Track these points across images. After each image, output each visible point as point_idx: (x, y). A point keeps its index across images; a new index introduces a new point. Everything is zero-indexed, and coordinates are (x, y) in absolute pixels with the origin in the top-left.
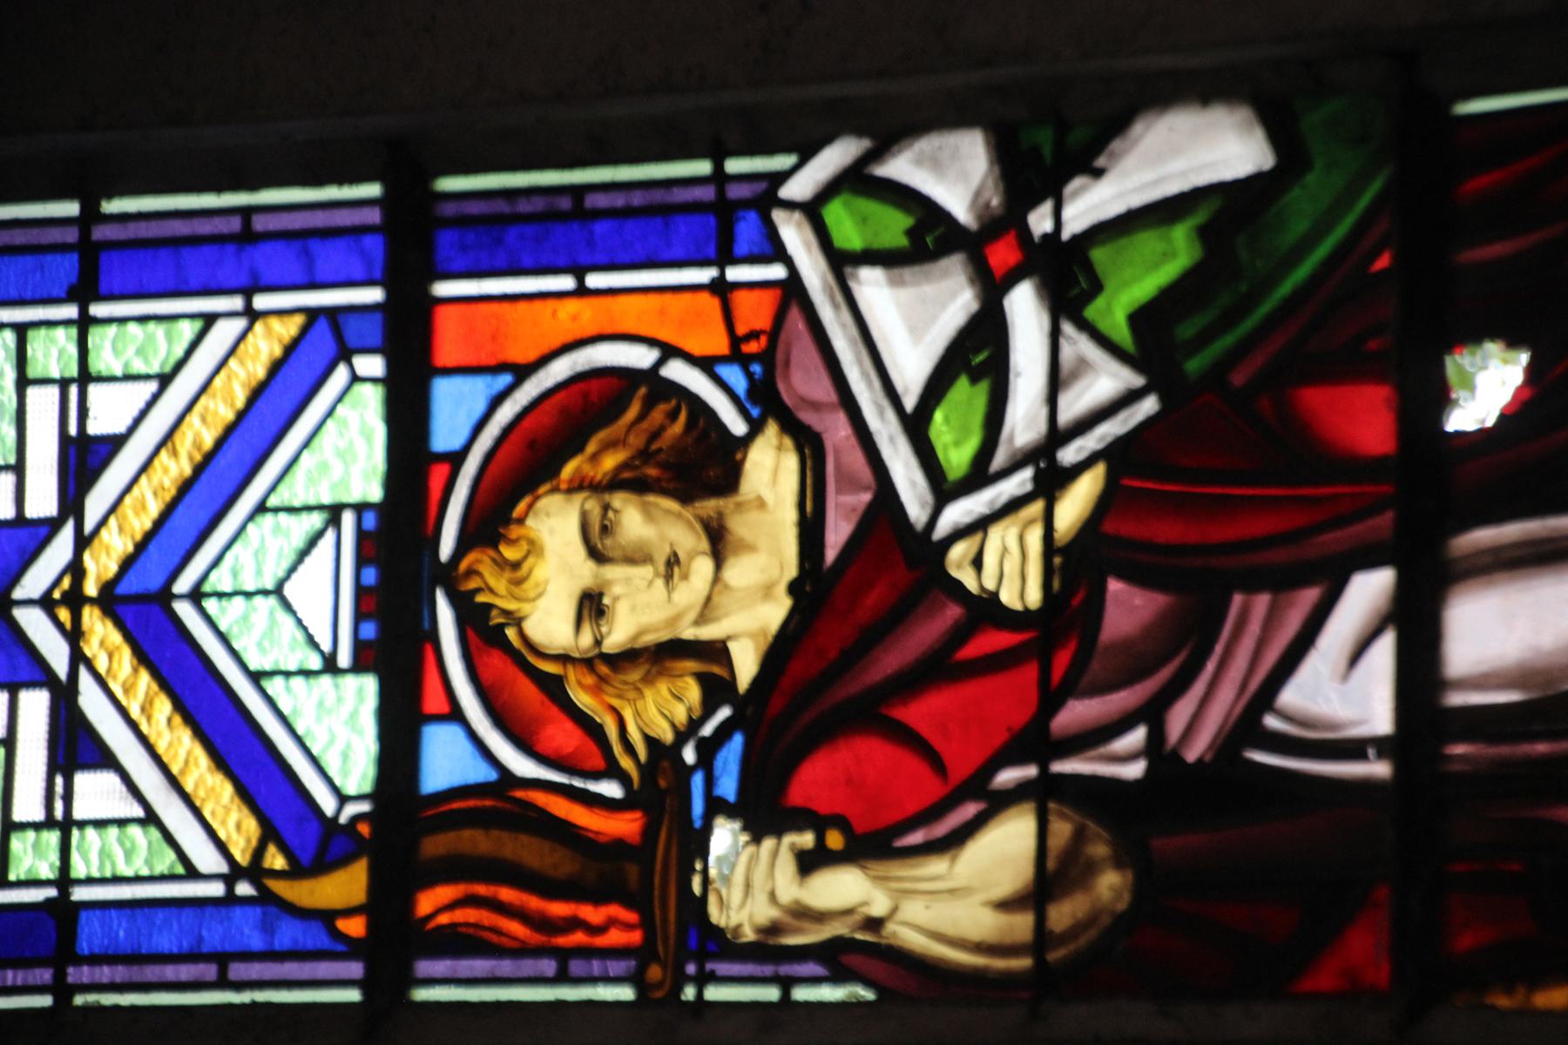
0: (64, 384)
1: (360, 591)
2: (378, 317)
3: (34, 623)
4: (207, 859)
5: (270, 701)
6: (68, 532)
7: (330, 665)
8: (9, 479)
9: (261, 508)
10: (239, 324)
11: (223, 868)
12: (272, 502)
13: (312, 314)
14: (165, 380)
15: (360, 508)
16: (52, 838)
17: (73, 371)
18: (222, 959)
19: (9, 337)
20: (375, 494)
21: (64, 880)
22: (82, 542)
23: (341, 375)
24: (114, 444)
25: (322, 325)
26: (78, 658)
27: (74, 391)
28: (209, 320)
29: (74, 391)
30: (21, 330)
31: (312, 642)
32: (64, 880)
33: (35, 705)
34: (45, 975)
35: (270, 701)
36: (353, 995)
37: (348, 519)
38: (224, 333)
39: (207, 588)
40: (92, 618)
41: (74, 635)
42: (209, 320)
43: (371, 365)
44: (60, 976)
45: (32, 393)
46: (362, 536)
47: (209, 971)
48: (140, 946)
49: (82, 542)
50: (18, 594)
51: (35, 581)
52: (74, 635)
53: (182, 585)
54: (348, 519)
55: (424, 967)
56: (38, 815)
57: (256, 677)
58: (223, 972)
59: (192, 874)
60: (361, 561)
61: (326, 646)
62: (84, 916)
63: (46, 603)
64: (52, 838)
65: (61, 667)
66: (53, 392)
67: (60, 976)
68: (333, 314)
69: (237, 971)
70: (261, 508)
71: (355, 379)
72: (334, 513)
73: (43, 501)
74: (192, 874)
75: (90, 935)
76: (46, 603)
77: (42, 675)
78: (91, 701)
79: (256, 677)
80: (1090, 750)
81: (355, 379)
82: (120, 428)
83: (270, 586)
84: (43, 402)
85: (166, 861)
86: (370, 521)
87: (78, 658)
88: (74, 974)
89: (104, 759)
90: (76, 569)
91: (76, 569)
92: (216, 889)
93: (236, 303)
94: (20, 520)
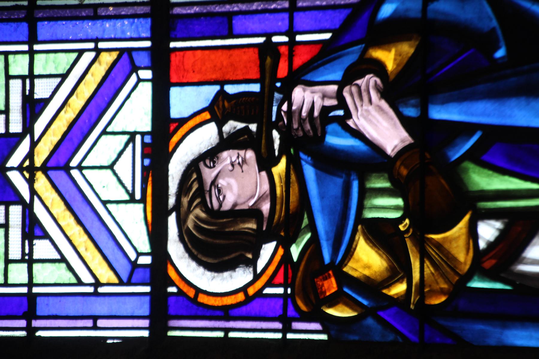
0: (23, 78)
1: (144, 169)
2: (148, 270)
3: (15, 177)
4: (87, 278)
5: (110, 213)
6: (27, 140)
7: (132, 200)
8: (3, 116)
9: (104, 132)
10: (93, 54)
11: (92, 281)
12: (109, 130)
13: (122, 51)
14: (64, 77)
15: (143, 134)
16: (25, 266)
17: (26, 73)
18: (95, 318)
19: (2, 57)
20: (147, 127)
21: (30, 284)
22: (34, 144)
23: (133, 79)
24: (45, 102)
25: (125, 56)
26: (33, 192)
27: (28, 81)
28: (81, 52)
29: (28, 81)
30: (6, 54)
31: (127, 191)
32: (30, 284)
33: (16, 211)
34: (23, 323)
35: (110, 213)
36: (145, 334)
37: (138, 138)
38: (88, 57)
39: (84, 164)
40: (40, 175)
41: (31, 182)
42: (81, 52)
43: (147, 74)
44: (29, 324)
45: (12, 82)
46: (144, 145)
47: (89, 323)
48: (47, 324)
49: (34, 144)
50: (8, 165)
51: (15, 160)
52: (31, 182)
53: (74, 163)
54: (138, 138)
55: (173, 323)
56: (18, 256)
57: (105, 203)
58: (95, 323)
59: (80, 283)
60: (144, 156)
61: (130, 188)
62: (39, 299)
63: (20, 168)
64: (25, 266)
65: (26, 196)
66: (19, 82)
67: (29, 324)
68: (129, 51)
69: (101, 323)
70: (104, 132)
71: (139, 80)
72: (132, 135)
73: (16, 127)
74: (80, 283)
75: (42, 308)
76: (20, 168)
77: (18, 200)
78: (38, 210)
79: (105, 203)
80: (190, 244)
81: (139, 80)
82: (47, 95)
83: (106, 164)
84: (16, 86)
85: (69, 278)
86: (148, 139)
87: (33, 192)
88: (36, 323)
89: (45, 236)
90: (30, 155)
91: (30, 155)
92: (91, 290)
93: (91, 45)
94: (7, 134)
